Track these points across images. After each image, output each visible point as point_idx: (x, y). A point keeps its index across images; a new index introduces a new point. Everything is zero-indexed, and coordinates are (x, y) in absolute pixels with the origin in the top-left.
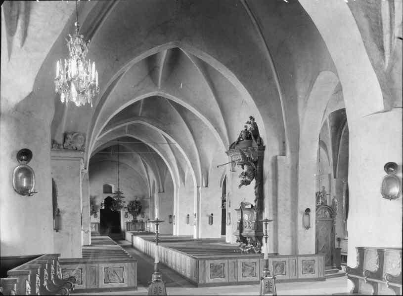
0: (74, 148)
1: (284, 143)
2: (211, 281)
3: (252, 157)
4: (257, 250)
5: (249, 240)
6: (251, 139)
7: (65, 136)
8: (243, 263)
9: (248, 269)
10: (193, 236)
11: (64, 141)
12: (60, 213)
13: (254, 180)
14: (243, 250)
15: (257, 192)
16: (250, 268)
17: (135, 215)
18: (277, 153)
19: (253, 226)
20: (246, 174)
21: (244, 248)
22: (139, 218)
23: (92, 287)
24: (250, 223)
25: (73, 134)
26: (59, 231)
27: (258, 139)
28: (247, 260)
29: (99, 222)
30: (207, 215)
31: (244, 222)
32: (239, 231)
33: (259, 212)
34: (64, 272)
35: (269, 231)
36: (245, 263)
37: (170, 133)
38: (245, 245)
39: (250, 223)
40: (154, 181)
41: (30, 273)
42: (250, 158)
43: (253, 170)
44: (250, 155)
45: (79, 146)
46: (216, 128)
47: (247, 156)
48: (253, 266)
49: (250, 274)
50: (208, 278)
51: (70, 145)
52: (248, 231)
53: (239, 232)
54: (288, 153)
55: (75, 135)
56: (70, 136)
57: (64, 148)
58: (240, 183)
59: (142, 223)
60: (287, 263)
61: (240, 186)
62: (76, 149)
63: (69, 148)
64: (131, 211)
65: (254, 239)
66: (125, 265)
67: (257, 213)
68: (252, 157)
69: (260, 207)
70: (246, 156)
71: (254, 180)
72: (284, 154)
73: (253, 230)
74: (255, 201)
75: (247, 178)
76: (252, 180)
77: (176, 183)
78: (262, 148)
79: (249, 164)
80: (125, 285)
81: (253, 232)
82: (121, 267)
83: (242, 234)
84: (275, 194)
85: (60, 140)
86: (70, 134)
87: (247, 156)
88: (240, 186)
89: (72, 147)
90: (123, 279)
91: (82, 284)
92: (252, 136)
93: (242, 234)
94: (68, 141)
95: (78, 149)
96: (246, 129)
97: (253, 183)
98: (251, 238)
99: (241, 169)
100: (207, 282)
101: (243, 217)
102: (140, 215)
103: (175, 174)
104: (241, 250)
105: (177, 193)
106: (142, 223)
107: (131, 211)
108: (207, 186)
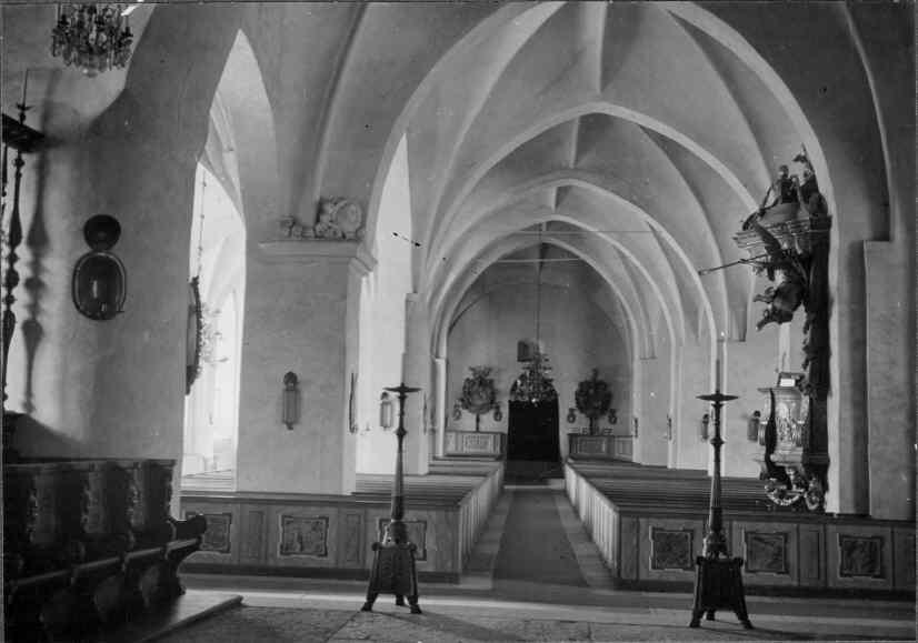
0: (340, 235)
1: (886, 205)
2: (655, 575)
3: (797, 247)
4: (813, 503)
5: (791, 473)
6: (797, 200)
7: (320, 211)
8: (746, 534)
9: (38, 469)
10: (706, 472)
11: (318, 220)
12: (299, 387)
13: (802, 308)
14: (776, 501)
15: (808, 341)
16: (771, 549)
17: (593, 418)
18: (865, 232)
19: (797, 434)
20: (779, 293)
21: (782, 495)
22: (603, 423)
23: (350, 565)
24: (794, 426)
25: (335, 204)
26: (294, 426)
27: (813, 198)
28: (762, 527)
29: (505, 430)
30: (744, 417)
31: (777, 423)
32: (764, 448)
33: (814, 396)
34: (288, 523)
35: (732, 432)
36: (752, 533)
37: (646, 206)
38: (784, 487)
39: (794, 426)
40: (785, 354)
41: (236, 516)
42: (792, 249)
43: (795, 281)
44: (791, 243)
45: (349, 228)
46: (745, 186)
47: (785, 246)
48: (778, 543)
49: (769, 566)
50: (647, 567)
51: (330, 228)
52: (789, 451)
53: (764, 452)
54: (898, 231)
55: (342, 204)
56: (329, 208)
57: (316, 237)
58: (762, 318)
59: (611, 438)
60: (888, 545)
61: (760, 325)
62: (344, 236)
63: (326, 235)
64: (583, 405)
65: (802, 470)
66: (430, 516)
67: (811, 399)
68: (797, 247)
69: (817, 384)
70: (779, 246)
71: (802, 308)
72: (884, 235)
73: (798, 445)
74: (805, 366)
75: (778, 304)
76: (795, 308)
77: (674, 327)
78: (822, 222)
79: (787, 267)
80: (329, 562)
81: (800, 451)
82: (419, 521)
83: (772, 457)
84: (858, 344)
85: (307, 217)
86: (328, 201)
87: (785, 246)
88: (760, 325)
89: (335, 233)
90: (425, 551)
91: (326, 554)
92: (799, 194)
93: (772, 457)
94: (325, 218)
95: (348, 236)
96: (785, 175)
97: (801, 315)
98: (795, 468)
99: (767, 279)
100: (643, 577)
101: (777, 409)
102: (606, 418)
103: (717, 314)
104: (772, 502)
105: (677, 357)
106: (611, 438)
107: (583, 405)
108: (743, 339)
